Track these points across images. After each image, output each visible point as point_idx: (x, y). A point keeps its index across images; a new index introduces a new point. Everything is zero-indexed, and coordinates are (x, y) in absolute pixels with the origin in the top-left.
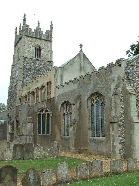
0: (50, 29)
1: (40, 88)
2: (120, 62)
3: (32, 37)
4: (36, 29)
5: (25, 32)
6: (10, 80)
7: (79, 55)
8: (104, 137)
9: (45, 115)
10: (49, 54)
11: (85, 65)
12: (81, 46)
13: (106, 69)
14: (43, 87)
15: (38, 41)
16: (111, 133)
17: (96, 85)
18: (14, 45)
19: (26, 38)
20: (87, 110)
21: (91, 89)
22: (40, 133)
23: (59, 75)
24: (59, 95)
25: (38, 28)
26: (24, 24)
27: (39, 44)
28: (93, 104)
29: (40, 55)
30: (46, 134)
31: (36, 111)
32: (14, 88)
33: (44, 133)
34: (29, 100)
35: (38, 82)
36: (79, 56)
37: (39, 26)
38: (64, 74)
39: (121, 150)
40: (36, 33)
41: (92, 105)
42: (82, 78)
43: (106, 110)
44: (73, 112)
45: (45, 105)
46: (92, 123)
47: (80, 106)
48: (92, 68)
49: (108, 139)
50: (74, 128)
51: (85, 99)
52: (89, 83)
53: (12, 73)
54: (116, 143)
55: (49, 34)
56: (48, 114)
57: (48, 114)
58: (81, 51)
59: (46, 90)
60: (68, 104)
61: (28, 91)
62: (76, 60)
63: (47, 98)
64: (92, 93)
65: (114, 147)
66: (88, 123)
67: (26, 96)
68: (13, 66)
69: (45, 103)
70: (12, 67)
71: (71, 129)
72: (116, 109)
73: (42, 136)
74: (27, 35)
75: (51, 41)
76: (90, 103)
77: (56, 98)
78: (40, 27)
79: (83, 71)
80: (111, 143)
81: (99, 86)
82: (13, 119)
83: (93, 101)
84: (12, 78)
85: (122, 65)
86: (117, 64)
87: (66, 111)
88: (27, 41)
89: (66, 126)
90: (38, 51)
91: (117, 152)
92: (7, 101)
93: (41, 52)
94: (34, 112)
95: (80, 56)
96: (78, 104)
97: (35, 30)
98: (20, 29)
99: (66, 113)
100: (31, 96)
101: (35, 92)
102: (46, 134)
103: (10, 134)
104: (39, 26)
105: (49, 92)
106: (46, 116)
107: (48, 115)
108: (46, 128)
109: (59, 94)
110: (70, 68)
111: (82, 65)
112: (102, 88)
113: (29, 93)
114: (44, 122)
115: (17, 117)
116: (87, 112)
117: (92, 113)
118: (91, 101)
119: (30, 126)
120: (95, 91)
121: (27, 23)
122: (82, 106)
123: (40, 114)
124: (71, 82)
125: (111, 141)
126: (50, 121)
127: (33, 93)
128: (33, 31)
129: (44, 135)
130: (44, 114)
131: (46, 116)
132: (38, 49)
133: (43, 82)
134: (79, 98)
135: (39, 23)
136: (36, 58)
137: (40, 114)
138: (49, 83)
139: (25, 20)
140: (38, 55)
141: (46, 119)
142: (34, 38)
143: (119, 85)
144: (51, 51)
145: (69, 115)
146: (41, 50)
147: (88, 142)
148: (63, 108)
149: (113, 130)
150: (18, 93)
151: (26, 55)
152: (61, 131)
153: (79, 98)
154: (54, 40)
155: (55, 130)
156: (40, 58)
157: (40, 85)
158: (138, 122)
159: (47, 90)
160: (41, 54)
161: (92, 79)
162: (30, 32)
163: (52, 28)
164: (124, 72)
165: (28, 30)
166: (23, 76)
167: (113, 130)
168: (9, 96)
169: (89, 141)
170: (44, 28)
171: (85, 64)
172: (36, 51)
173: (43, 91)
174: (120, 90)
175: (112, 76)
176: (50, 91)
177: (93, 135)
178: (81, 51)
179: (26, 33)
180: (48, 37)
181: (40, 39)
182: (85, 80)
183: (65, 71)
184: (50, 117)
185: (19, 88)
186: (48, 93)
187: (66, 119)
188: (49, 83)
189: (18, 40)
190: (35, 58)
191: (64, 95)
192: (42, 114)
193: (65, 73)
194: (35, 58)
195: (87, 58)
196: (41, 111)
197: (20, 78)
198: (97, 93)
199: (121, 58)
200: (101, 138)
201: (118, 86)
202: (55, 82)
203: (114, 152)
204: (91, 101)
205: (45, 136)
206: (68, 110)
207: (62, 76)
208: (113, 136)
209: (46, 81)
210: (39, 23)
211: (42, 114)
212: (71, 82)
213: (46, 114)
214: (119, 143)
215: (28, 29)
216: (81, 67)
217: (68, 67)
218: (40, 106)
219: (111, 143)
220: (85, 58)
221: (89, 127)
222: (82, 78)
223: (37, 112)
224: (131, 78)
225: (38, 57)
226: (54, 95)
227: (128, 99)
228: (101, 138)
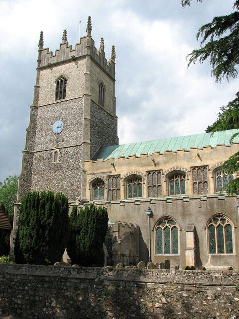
101: (106, 182)
160: (105, 100)
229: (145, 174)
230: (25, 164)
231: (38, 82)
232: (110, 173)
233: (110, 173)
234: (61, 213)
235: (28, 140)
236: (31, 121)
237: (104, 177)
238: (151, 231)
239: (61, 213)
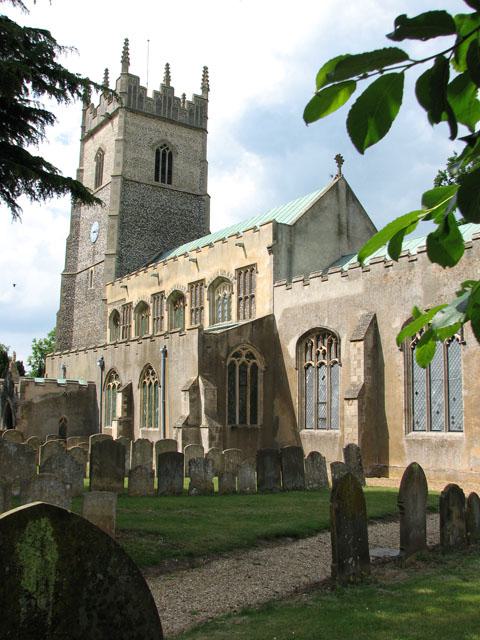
4: (158, 89)
7: (335, 188)
8: (460, 434)
9: (246, 367)
14: (220, 281)
23: (284, 246)
24: (286, 311)
25: (167, 88)
26: (125, 73)
27: (170, 139)
29: (170, 172)
30: (249, 423)
31: (223, 354)
36: (335, 194)
37: (168, 78)
38: (296, 246)
40: (191, 114)
44: (356, 362)
48: (368, 229)
51: (394, 326)
55: (200, 106)
56: (254, 364)
57: (254, 364)
61: (156, 289)
62: (326, 202)
67: (143, 307)
75: (205, 131)
77: (278, 317)
79: (345, 236)
90: (164, 161)
92: (56, 317)
93: (174, 165)
94: (218, 357)
95: (337, 190)
97: (156, 93)
101: (188, 295)
104: (168, 78)
105: (247, 299)
106: (249, 370)
107: (255, 367)
109: (287, 304)
110: (312, 227)
111: (344, 219)
121: (132, 70)
126: (260, 387)
127: (177, 298)
128: (150, 94)
129: (244, 425)
130: (244, 365)
131: (249, 370)
132: (164, 155)
135: (168, 72)
136: (160, 184)
139: (126, 61)
140: (163, 173)
141: (249, 378)
144: (204, 162)
145: (160, 390)
146: (174, 158)
154: (211, 125)
156: (170, 182)
157: (208, 275)
159: (239, 292)
160: (174, 171)
163: (206, 88)
165: (170, 101)
170: (186, 87)
172: (157, 161)
179: (129, 102)
181: (172, 122)
183: (298, 237)
184: (260, 375)
186: (240, 299)
193: (298, 240)
195: (355, 199)
199: (46, 33)
206: (324, 354)
210: (168, 72)
211: (238, 364)
213: (250, 365)
215: (135, 88)
216: (340, 224)
217: (307, 225)
220: (351, 199)
223: (225, 360)
225: (163, 182)
229: (233, 273)
230: (64, 295)
231: (81, 164)
232: (124, 299)
233: (124, 299)
234: (365, 605)
235: (68, 257)
236: (72, 227)
237: (148, 299)
238: (320, 379)
239: (365, 605)
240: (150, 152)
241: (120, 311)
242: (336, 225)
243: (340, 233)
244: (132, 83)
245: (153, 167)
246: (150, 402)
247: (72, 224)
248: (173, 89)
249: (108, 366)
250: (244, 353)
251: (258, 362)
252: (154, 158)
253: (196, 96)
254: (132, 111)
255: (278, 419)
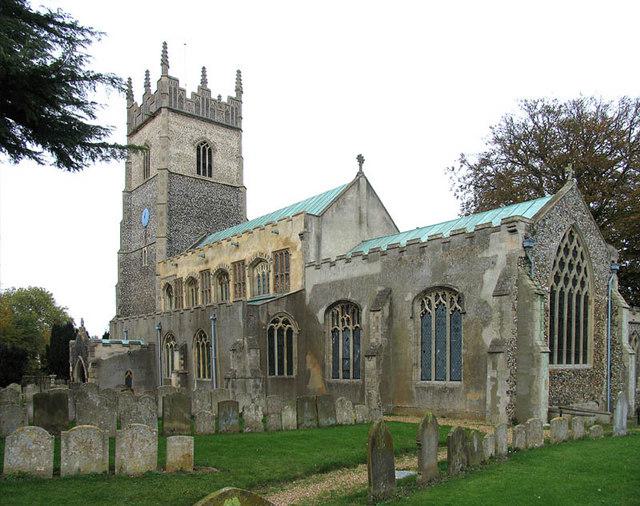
0: (234, 95)
1: (247, 263)
2: (515, 224)
3: (218, 124)
4: (196, 91)
5: (167, 97)
6: (122, 231)
7: (356, 183)
9: (283, 330)
10: (234, 166)
11: (371, 211)
12: (361, 159)
13: (471, 237)
14: (258, 261)
15: (204, 126)
16: (489, 372)
17: (440, 269)
18: (126, 133)
19: (172, 117)
20: (410, 325)
21: (425, 277)
22: (272, 372)
24: (315, 287)
26: (165, 73)
28: (426, 311)
29: (210, 166)
30: (286, 374)
32: (136, 254)
33: (281, 372)
34: (206, 292)
35: (242, 246)
37: (204, 81)
39: (510, 406)
40: (197, 104)
41: (425, 314)
42: (397, 250)
43: (466, 327)
45: (282, 308)
46: (423, 352)
47: (391, 315)
49: (480, 385)
50: (378, 363)
52: (421, 265)
53: (124, 213)
54: (501, 393)
58: (360, 174)
59: (272, 269)
60: (348, 307)
61: (202, 267)
63: (275, 289)
64: (428, 285)
65: (496, 400)
66: (412, 351)
67: (192, 281)
68: (128, 193)
69: (283, 303)
70: (124, 197)
71: (370, 364)
72: (501, 324)
73: (276, 379)
74: (177, 108)
75: (240, 130)
76: (418, 310)
77: (308, 290)
78: (209, 86)
80: (489, 392)
81: (450, 272)
82: (187, 337)
83: (429, 304)
84: (126, 226)
85: (519, 231)
86: (504, 229)
87: (341, 323)
88: (174, 127)
89: (341, 357)
91: (502, 409)
93: (214, 160)
96: (386, 309)
97: (193, 94)
98: (147, 85)
99: (340, 328)
100: (213, 280)
102: (286, 374)
103: (179, 374)
104: (204, 81)
105: (283, 275)
107: (290, 331)
108: (286, 361)
111: (364, 211)
112: (459, 277)
113: (205, 273)
114: (280, 347)
115: (202, 334)
116: (411, 329)
117: (425, 326)
118: (423, 304)
119: (252, 358)
120: (437, 283)
121: (171, 73)
122: (395, 314)
123: (272, 329)
124: (361, 258)
125: (489, 388)
127: (222, 274)
128: (189, 96)
130: (281, 330)
133: (259, 249)
134: (387, 295)
136: (201, 177)
137: (272, 329)
138: (282, 256)
139: (165, 63)
140: (204, 167)
142: (222, 125)
143: (510, 274)
144: (239, 158)
147: (412, 392)
148: (331, 317)
149: (494, 367)
150: (160, 269)
151: (176, 167)
152: (327, 368)
153: (387, 295)
154: (245, 125)
155: (305, 366)
156: (210, 176)
157: (247, 255)
158: (638, 321)
159: (276, 270)
160: (214, 166)
161: (428, 254)
162: (181, 98)
163: (239, 90)
164: (521, 248)
165: (207, 103)
166: (170, 225)
167: (494, 367)
168: (121, 274)
169: (415, 390)
170: (221, 88)
171: (104, 140)
172: (198, 156)
173: (259, 271)
174: (511, 286)
175: (490, 253)
176: (287, 274)
177: (425, 377)
178: (360, 174)
180: (228, 116)
181: (210, 122)
182: (405, 256)
185: (160, 257)
187: (341, 341)
188: (282, 256)
189: (140, 121)
190: (197, 176)
191: (341, 284)
192: (276, 329)
194: (197, 176)
196: (275, 321)
197: (163, 231)
198: (441, 288)
200: (448, 383)
201: (505, 277)
202: (305, 253)
203: (495, 410)
204: (423, 304)
205: (284, 379)
207: (319, 238)
208: (493, 379)
209: (270, 249)
211: (276, 329)
212: (361, 258)
213: (286, 329)
214: (507, 392)
218: (273, 310)
219: (489, 392)
221: (414, 361)
222: (397, 250)
224: (532, 259)
225: (204, 174)
226: (300, 283)
227: (530, 305)
228: (448, 383)
240: (192, 148)
241: (173, 284)
242: (358, 215)
243: (360, 223)
244: (170, 86)
245: (195, 163)
246: (205, 358)
247: (124, 210)
248: (209, 91)
249: (166, 328)
250: (282, 319)
251: (292, 327)
252: (195, 154)
253: (230, 98)
254: (174, 111)
255: (309, 371)
